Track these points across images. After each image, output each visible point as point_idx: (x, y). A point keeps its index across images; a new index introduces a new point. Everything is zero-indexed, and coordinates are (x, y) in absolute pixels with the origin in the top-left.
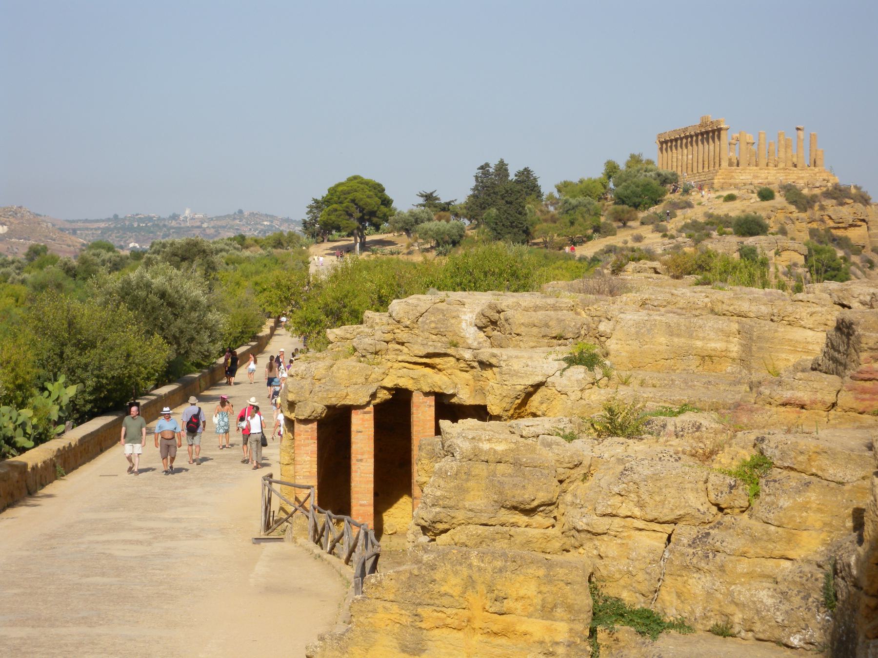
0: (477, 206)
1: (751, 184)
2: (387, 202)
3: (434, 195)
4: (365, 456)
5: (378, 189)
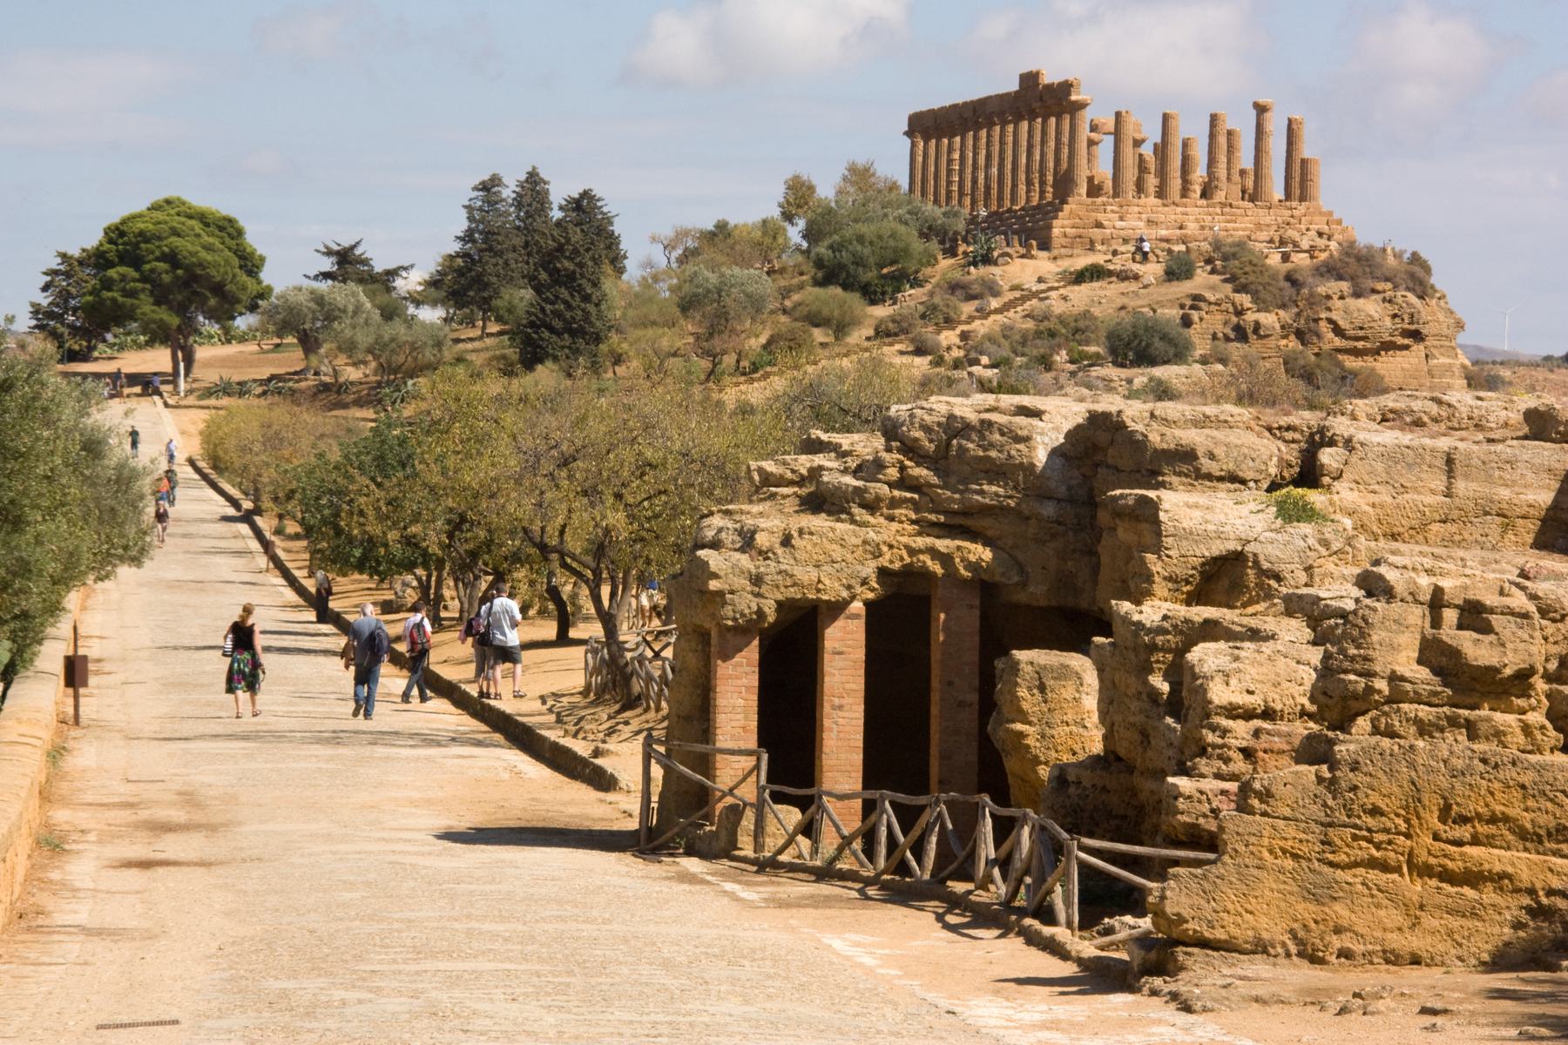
0: (462, 284)
1: (161, 517)
2: (251, 264)
3: (358, 252)
4: (847, 701)
5: (228, 229)
